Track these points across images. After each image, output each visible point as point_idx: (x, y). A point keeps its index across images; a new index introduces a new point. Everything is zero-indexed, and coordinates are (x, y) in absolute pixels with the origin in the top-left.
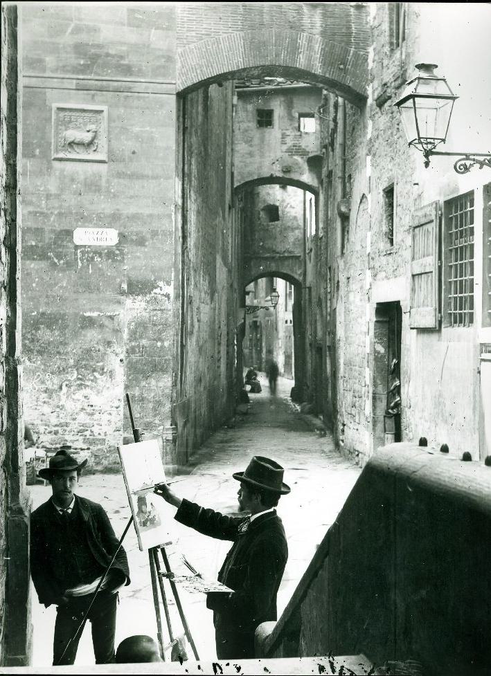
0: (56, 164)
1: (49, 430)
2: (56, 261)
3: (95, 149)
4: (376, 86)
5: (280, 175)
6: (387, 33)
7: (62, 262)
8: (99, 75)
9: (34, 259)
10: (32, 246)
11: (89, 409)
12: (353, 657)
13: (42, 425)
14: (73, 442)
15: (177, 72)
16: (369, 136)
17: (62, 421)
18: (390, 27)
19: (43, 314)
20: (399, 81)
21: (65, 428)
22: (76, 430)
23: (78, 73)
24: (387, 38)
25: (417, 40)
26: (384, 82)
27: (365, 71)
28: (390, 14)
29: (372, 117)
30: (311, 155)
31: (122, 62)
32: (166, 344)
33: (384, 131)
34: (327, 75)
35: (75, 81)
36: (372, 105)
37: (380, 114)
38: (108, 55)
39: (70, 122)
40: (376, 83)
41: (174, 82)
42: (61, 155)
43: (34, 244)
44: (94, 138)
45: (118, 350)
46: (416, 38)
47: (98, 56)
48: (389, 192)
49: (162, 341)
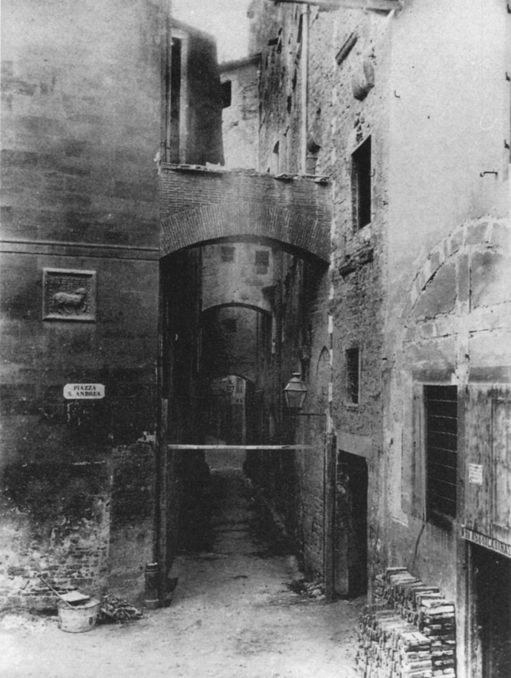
0: (47, 325)
1: (38, 574)
2: (46, 415)
3: (84, 309)
4: (339, 255)
5: (240, 301)
6: (350, 211)
7: (52, 416)
8: (88, 242)
9: (24, 414)
10: (23, 402)
11: (77, 553)
12: (156, 313)
13: (32, 570)
14: (60, 583)
15: (161, 240)
16: (331, 298)
17: (51, 565)
18: (353, 206)
19: (34, 465)
20: (366, 258)
21: (54, 571)
22: (64, 573)
23: (68, 240)
24: (351, 216)
25: (385, 225)
26: (347, 253)
27: (327, 241)
28: (353, 194)
29: (335, 282)
30: (265, 286)
31: (111, 230)
32: (149, 488)
33: (348, 297)
34: (295, 244)
35: (65, 248)
36: (334, 272)
37: (343, 281)
38: (97, 223)
39: (61, 285)
40: (339, 253)
41: (157, 249)
42: (51, 316)
43: (25, 399)
44: (83, 300)
45: (105, 496)
46: (384, 223)
47: (88, 224)
48: (353, 354)
49: (146, 486)
